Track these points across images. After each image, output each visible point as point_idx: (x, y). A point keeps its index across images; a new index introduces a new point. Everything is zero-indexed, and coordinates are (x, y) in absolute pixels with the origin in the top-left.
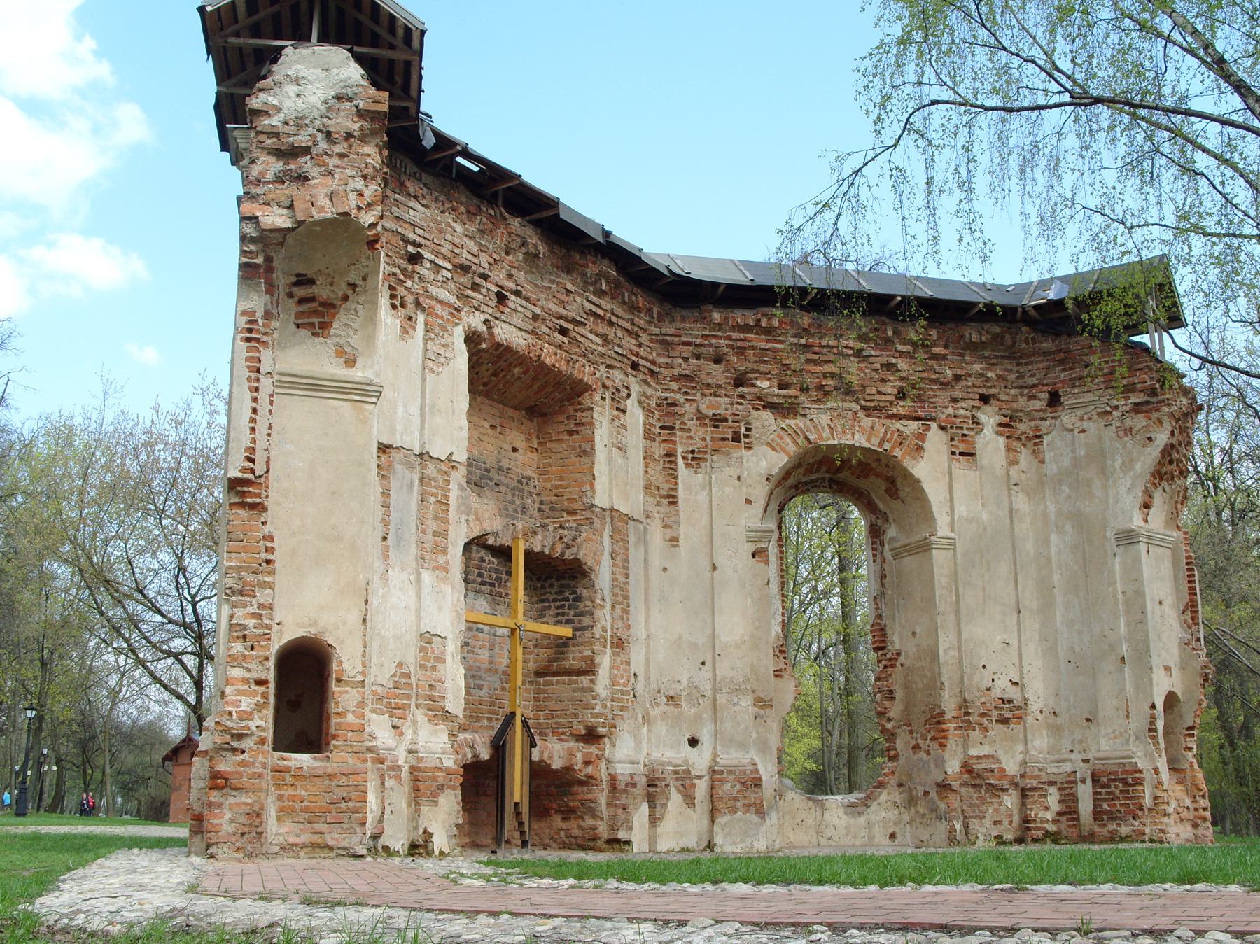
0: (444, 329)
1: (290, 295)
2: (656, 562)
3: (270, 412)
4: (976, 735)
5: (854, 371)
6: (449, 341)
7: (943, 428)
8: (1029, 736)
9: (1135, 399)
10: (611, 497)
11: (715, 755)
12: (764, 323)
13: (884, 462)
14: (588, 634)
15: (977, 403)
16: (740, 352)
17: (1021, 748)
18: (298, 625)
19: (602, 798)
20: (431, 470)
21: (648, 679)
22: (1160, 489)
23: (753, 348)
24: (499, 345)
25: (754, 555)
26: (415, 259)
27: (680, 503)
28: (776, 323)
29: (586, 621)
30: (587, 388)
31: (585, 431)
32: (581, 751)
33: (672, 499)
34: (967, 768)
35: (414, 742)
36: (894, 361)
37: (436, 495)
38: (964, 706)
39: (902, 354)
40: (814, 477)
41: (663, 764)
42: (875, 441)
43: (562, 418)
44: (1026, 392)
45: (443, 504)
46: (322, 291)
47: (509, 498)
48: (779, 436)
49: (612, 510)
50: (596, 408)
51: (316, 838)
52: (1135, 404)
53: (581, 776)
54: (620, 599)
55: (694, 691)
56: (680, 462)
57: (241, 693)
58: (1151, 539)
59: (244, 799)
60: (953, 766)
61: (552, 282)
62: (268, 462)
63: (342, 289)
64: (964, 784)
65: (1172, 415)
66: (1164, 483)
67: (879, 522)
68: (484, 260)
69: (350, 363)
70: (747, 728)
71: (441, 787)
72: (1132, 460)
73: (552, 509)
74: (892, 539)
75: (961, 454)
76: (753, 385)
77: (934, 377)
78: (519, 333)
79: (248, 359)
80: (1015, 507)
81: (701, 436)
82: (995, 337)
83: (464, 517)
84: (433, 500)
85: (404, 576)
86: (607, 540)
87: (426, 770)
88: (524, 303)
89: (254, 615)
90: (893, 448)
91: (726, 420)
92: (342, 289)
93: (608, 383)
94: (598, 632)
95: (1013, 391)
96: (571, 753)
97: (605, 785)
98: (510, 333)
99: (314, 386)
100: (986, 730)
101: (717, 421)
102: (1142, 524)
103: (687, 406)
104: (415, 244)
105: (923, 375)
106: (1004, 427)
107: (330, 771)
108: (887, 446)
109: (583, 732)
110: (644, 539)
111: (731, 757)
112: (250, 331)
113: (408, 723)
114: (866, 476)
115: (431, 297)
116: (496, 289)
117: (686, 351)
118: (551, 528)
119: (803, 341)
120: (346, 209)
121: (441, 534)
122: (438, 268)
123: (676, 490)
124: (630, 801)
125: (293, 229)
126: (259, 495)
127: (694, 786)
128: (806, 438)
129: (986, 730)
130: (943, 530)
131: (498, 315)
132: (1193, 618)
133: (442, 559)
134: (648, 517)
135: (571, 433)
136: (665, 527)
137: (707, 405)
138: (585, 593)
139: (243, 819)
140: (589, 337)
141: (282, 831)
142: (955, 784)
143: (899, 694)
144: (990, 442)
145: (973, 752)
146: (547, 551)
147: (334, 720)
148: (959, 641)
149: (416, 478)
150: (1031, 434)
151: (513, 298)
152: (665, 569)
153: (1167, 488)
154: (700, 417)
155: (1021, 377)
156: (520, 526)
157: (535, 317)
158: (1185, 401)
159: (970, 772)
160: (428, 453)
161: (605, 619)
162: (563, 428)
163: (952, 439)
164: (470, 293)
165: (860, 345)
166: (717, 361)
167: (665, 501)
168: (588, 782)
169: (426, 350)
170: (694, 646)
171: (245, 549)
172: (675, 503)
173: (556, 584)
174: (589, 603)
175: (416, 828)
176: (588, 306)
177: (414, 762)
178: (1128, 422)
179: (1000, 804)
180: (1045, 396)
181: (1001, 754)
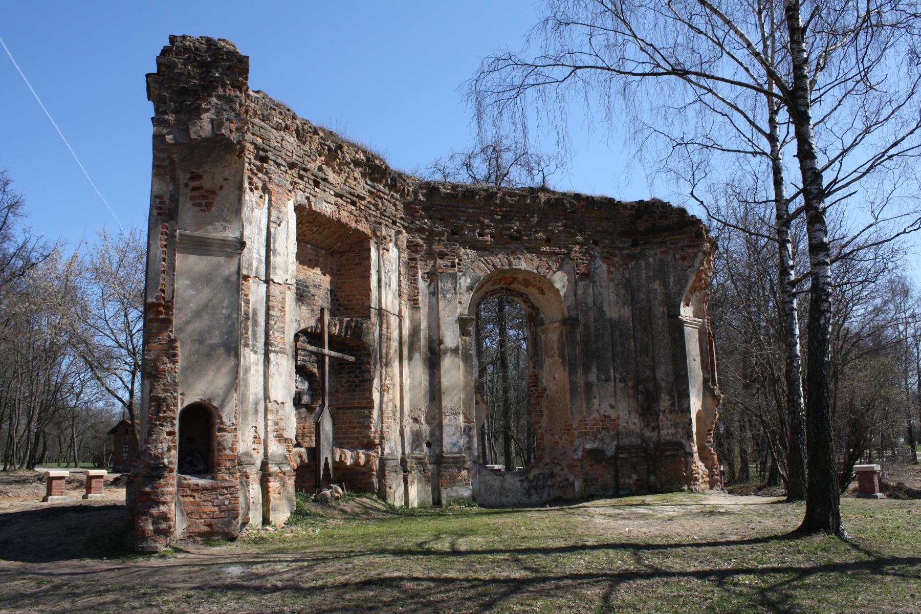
1: (186, 185)
26: (264, 160)
73: (346, 309)
98: (326, 207)
116: (313, 178)
122: (279, 165)
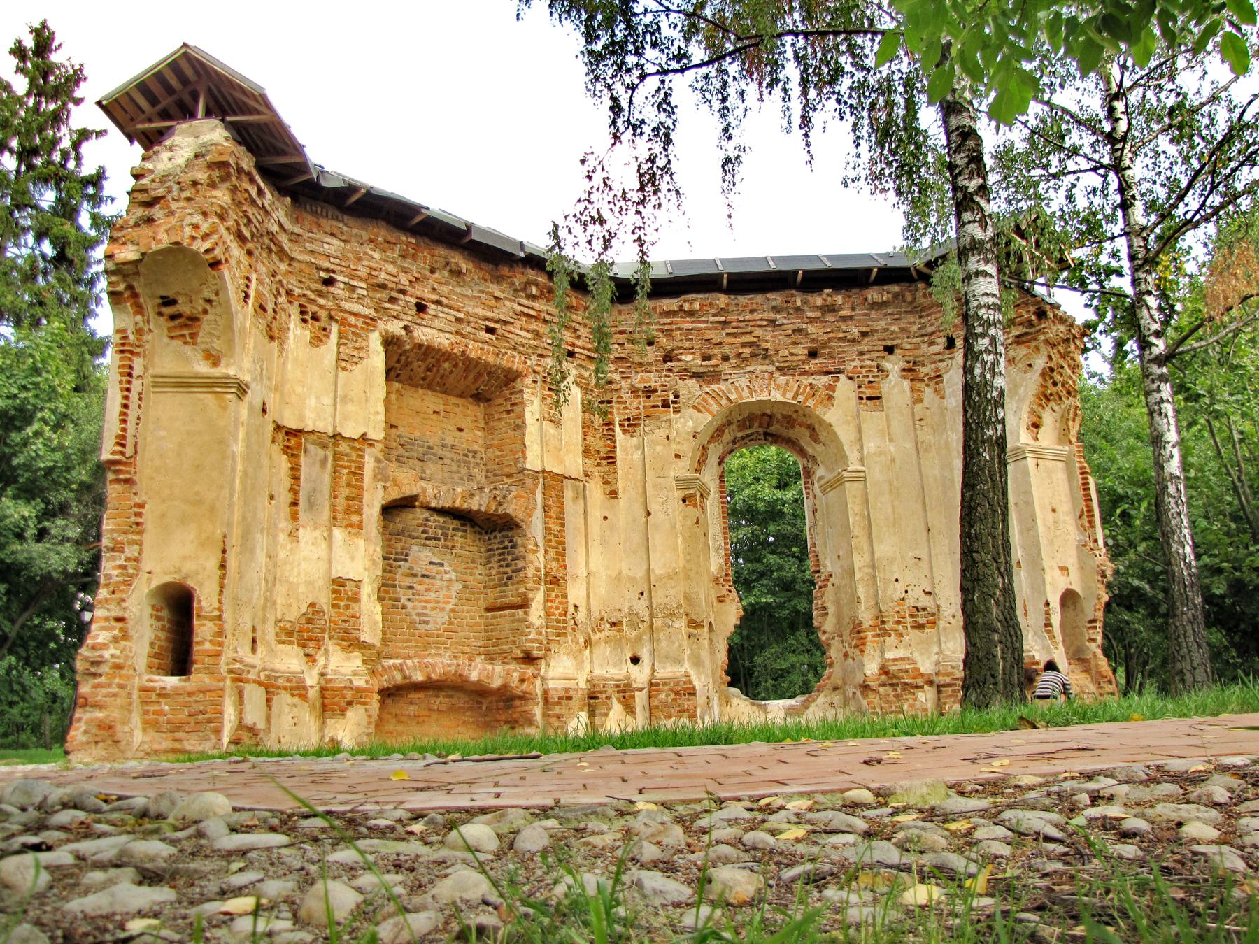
0: (359, 335)
1: (160, 314)
2: (596, 514)
3: (139, 406)
4: (891, 640)
5: (768, 338)
6: (364, 344)
7: (851, 378)
8: (943, 639)
9: (1016, 331)
10: (542, 461)
11: (653, 670)
12: (686, 307)
13: (801, 412)
14: (522, 574)
15: (882, 354)
16: (668, 333)
17: (936, 649)
18: (165, 574)
19: (538, 711)
20: (344, 447)
21: (589, 610)
22: (1048, 410)
23: (679, 329)
24: (420, 346)
25: (684, 501)
26: (329, 282)
27: (618, 462)
28: (697, 306)
29: (520, 564)
30: (517, 375)
31: (518, 409)
32: (516, 671)
33: (611, 460)
34: (884, 670)
35: (325, 667)
36: (804, 326)
37: (349, 467)
38: (880, 618)
39: (812, 321)
40: (748, 432)
41: (606, 679)
42: (790, 395)
43: (501, 401)
44: (926, 339)
45: (358, 473)
46: (183, 307)
47: (455, 468)
48: (704, 400)
49: (544, 471)
50: (526, 390)
51: (177, 745)
52: (1017, 337)
53: (518, 692)
54: (554, 544)
55: (635, 618)
56: (618, 429)
57: (103, 629)
58: (1040, 455)
59: (99, 715)
60: (871, 668)
61: (482, 292)
62: (136, 446)
63: (200, 305)
64: (883, 685)
65: (1047, 342)
66: (1052, 404)
67: (810, 465)
68: (404, 279)
69: (215, 364)
70: (680, 646)
71: (350, 703)
72: (1016, 386)
73: (495, 475)
74: (821, 478)
75: (868, 398)
76: (679, 360)
77: (841, 335)
78: (442, 335)
79: (120, 367)
80: (920, 438)
81: (635, 406)
82: (896, 296)
83: (381, 484)
84: (345, 471)
85: (317, 533)
86: (539, 497)
87: (333, 689)
88: (446, 310)
89: (120, 567)
90: (806, 400)
91: (655, 391)
92: (200, 305)
93: (537, 368)
94: (530, 572)
95: (914, 340)
96: (508, 673)
97: (540, 698)
99: (184, 384)
100: (901, 635)
101: (649, 392)
102: (1032, 442)
103: (623, 383)
104: (327, 270)
105: (830, 335)
106: (910, 370)
107: (189, 689)
108: (801, 398)
109: (521, 655)
110: (581, 495)
111: (666, 671)
112: (123, 344)
113: (321, 652)
114: (793, 427)
115: (345, 311)
117: (622, 338)
118: (487, 490)
119: (723, 319)
120: (179, 239)
121: (356, 496)
122: (353, 288)
123: (614, 452)
124: (564, 711)
125: (140, 261)
126: (128, 472)
127: (633, 697)
128: (728, 399)
129: (901, 635)
130: (854, 466)
131: (419, 321)
132: (1090, 522)
133: (355, 518)
134: (587, 476)
135: (508, 412)
136: (605, 483)
137: (638, 379)
138: (519, 541)
139: (94, 731)
140: (519, 333)
141: (147, 739)
142: (874, 685)
143: (831, 610)
144: (895, 387)
145: (889, 655)
146: (483, 509)
147: (195, 648)
148: (873, 560)
149: (330, 454)
150: (933, 375)
151: (434, 307)
152: (605, 518)
153: (1056, 407)
154: (634, 391)
155: (922, 327)
156: (459, 490)
157: (458, 320)
158: (1062, 328)
159: (887, 673)
160: (340, 434)
161: (538, 561)
162: (502, 409)
163: (859, 387)
164: (387, 305)
165: (772, 315)
166: (650, 344)
167: (604, 462)
168: (524, 697)
169: (339, 353)
170: (633, 580)
171: (119, 516)
172: (614, 463)
173: (499, 535)
174: (522, 549)
175: (323, 737)
176: (519, 309)
177: (323, 682)
178: (1011, 353)
179: (915, 700)
180: (942, 341)
181: (916, 656)
